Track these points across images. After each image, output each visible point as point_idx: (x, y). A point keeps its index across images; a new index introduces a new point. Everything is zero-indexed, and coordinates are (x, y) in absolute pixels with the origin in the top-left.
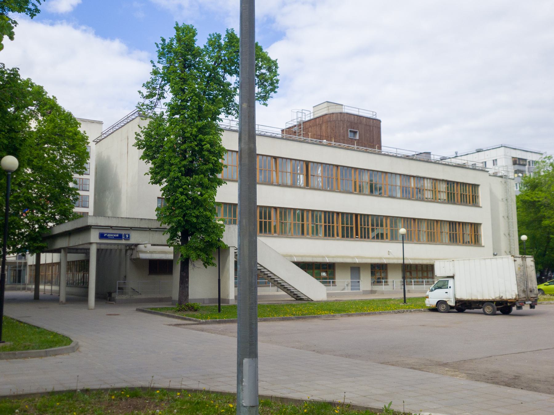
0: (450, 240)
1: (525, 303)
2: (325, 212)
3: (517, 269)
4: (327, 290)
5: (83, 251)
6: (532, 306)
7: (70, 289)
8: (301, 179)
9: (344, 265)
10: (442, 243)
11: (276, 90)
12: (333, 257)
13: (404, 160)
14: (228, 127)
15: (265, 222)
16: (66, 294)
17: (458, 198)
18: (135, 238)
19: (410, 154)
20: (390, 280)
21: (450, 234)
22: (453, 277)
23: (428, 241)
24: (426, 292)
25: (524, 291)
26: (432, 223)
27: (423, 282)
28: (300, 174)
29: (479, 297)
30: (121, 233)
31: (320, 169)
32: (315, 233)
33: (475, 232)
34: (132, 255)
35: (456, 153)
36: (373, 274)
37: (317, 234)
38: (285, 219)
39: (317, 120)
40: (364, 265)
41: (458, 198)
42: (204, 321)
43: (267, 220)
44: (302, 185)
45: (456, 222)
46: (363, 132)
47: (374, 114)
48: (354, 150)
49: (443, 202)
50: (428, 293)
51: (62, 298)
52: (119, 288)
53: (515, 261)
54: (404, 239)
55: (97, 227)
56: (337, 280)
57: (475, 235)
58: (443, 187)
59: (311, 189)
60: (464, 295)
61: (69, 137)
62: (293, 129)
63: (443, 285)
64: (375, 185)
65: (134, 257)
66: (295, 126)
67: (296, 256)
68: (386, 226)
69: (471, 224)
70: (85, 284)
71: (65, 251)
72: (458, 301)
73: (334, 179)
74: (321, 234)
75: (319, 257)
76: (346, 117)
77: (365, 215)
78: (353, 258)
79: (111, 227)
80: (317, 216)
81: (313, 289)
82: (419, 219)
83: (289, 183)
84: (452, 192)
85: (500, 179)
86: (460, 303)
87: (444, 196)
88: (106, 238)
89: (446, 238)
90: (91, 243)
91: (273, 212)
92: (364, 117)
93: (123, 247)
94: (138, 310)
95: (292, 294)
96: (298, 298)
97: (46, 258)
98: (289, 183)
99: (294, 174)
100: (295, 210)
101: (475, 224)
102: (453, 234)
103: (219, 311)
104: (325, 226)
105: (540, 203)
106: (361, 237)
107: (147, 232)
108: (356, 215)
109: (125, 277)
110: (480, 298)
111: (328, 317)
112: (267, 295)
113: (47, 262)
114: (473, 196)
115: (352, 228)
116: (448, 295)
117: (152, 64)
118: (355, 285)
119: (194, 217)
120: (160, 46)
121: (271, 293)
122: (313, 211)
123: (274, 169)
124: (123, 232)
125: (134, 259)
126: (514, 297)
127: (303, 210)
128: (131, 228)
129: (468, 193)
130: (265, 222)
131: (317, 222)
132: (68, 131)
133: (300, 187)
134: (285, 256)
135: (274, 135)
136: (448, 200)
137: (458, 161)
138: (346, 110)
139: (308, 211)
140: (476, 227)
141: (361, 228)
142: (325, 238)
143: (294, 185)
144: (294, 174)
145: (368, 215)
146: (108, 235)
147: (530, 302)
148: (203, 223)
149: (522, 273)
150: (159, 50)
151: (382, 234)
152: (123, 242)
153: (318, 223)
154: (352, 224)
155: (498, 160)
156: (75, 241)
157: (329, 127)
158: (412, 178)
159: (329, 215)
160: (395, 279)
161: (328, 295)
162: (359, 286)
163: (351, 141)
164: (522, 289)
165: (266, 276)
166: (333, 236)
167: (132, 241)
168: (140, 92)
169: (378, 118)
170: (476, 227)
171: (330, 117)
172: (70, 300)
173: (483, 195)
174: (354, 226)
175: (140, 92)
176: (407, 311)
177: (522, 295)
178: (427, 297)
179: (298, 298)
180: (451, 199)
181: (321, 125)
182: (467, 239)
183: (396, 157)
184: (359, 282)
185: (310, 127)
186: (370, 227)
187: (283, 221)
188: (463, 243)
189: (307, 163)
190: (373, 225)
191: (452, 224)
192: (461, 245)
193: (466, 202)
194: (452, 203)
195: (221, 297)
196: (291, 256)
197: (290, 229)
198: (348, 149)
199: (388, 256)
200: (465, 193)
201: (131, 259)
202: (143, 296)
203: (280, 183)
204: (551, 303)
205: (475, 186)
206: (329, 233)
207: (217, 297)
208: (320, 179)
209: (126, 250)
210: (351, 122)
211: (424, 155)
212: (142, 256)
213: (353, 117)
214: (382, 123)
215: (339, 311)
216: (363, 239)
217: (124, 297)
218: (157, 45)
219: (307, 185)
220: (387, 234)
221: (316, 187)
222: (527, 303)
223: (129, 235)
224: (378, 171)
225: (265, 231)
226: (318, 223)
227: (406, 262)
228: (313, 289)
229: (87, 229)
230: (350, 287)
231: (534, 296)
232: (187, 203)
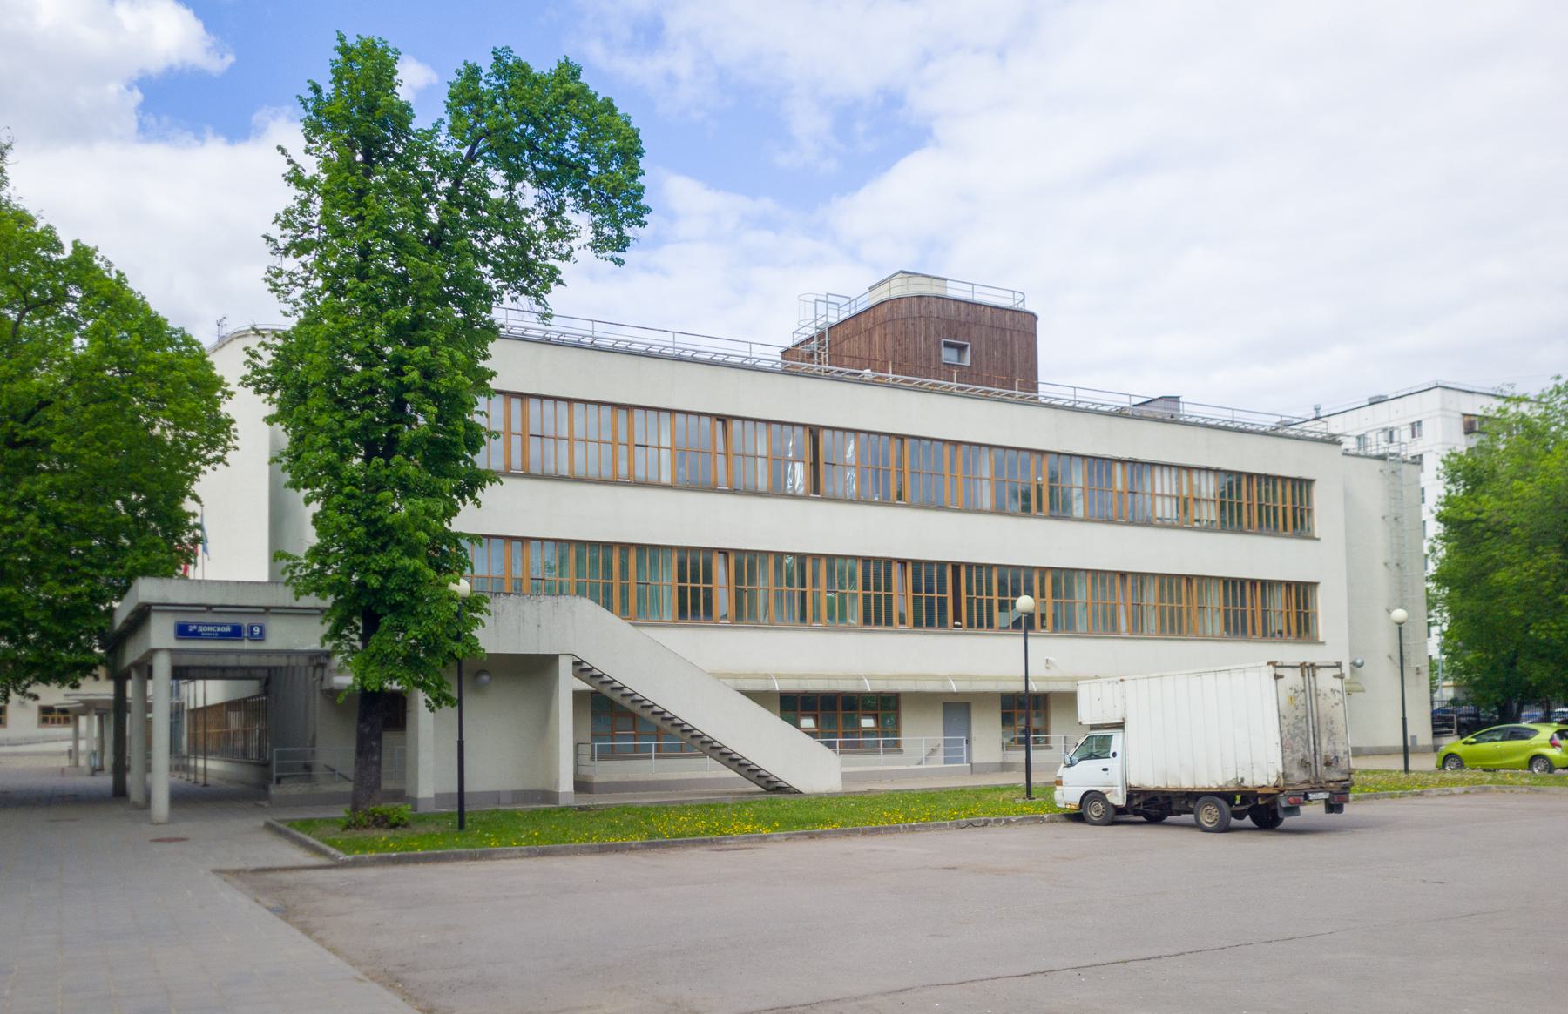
0: (1227, 628)
1: (1306, 797)
2: (866, 560)
3: (1284, 700)
4: (843, 764)
5: (238, 673)
6: (1333, 806)
8: (799, 475)
9: (924, 700)
10: (1205, 638)
11: (645, 218)
12: (888, 678)
14: (588, 341)
15: (695, 591)
17: (1250, 514)
19: (1124, 402)
21: (1226, 612)
22: (1120, 726)
23: (1163, 630)
24: (1056, 768)
25: (1304, 764)
26: (1172, 583)
28: (793, 461)
29: (1184, 781)
31: (852, 447)
32: (837, 616)
33: (1298, 606)
35: (1317, 409)
36: (1007, 719)
37: (843, 618)
38: (752, 580)
39: (863, 318)
40: (983, 697)
41: (1250, 514)
42: (350, 857)
43: (701, 585)
44: (801, 491)
45: (1243, 581)
46: (988, 346)
48: (951, 394)
49: (1209, 528)
50: (1062, 772)
53: (1277, 677)
54: (1026, 624)
55: (168, 608)
56: (905, 738)
57: (1298, 615)
59: (824, 499)
60: (1150, 779)
61: (146, 377)
62: (805, 349)
63: (1097, 746)
64: (1037, 487)
65: (326, 686)
66: (812, 338)
67: (779, 677)
69: (1288, 584)
72: (1132, 794)
73: (893, 474)
74: (855, 617)
75: (847, 677)
76: (933, 307)
77: (980, 566)
78: (944, 679)
79: (210, 607)
80: (842, 572)
81: (807, 762)
82: (1264, 583)
83: (762, 484)
84: (1235, 500)
85: (1379, 464)
86: (1142, 799)
87: (1210, 513)
88: (196, 635)
89: (1215, 623)
91: (896, 568)
94: (269, 827)
95: (754, 776)
96: (771, 786)
98: (762, 484)
99: (778, 463)
100: (780, 555)
102: (1235, 612)
103: (461, 825)
104: (866, 598)
105: (1482, 525)
106: (970, 625)
108: (956, 567)
110: (1187, 784)
112: (698, 780)
113: (210, 702)
114: (1294, 510)
115: (942, 602)
116: (1110, 778)
117: (285, 159)
119: (375, 572)
120: (310, 105)
121: (708, 775)
122: (831, 558)
123: (720, 448)
124: (245, 622)
126: (1273, 780)
127: (801, 558)
128: (267, 610)
129: (1280, 504)
130: (695, 591)
131: (842, 586)
132: (147, 363)
133: (794, 496)
134: (718, 676)
135: (719, 358)
136: (1223, 522)
137: (1319, 427)
138: (955, 291)
139: (817, 557)
140: (1302, 593)
141: (970, 602)
142: (867, 628)
143: (777, 491)
144: (778, 463)
145: (990, 567)
146: (201, 629)
147: (1326, 796)
148: (401, 589)
149: (1301, 713)
150: (309, 118)
153: (847, 590)
154: (942, 589)
155: (1424, 424)
157: (889, 337)
158: (1118, 466)
159: (877, 569)
161: (846, 777)
163: (946, 371)
164: (1299, 756)
168: (268, 238)
169: (1029, 307)
170: (1302, 593)
171: (891, 310)
173: (1325, 508)
174: (949, 595)
175: (268, 238)
176: (998, 821)
177: (1299, 775)
178: (1059, 783)
179: (773, 787)
181: (870, 332)
182: (1278, 623)
183: (1073, 409)
185: (847, 338)
186: (996, 598)
187: (745, 586)
188: (1265, 635)
189: (814, 431)
190: (1003, 592)
191: (1234, 586)
192: (1255, 641)
193: (1276, 526)
194: (1233, 531)
195: (467, 789)
196: (735, 677)
197: (767, 607)
198: (931, 392)
199: (1047, 674)
200: (1271, 503)
204: (1452, 794)
205: (1302, 485)
206: (877, 616)
207: (456, 790)
208: (851, 474)
210: (950, 322)
211: (1161, 403)
213: (953, 307)
214: (1039, 323)
218: (304, 103)
219: (815, 488)
221: (840, 493)
222: (1312, 796)
224: (932, 440)
225: (695, 614)
226: (847, 590)
227: (1034, 687)
230: (940, 755)
231: (1337, 777)
232: (352, 535)
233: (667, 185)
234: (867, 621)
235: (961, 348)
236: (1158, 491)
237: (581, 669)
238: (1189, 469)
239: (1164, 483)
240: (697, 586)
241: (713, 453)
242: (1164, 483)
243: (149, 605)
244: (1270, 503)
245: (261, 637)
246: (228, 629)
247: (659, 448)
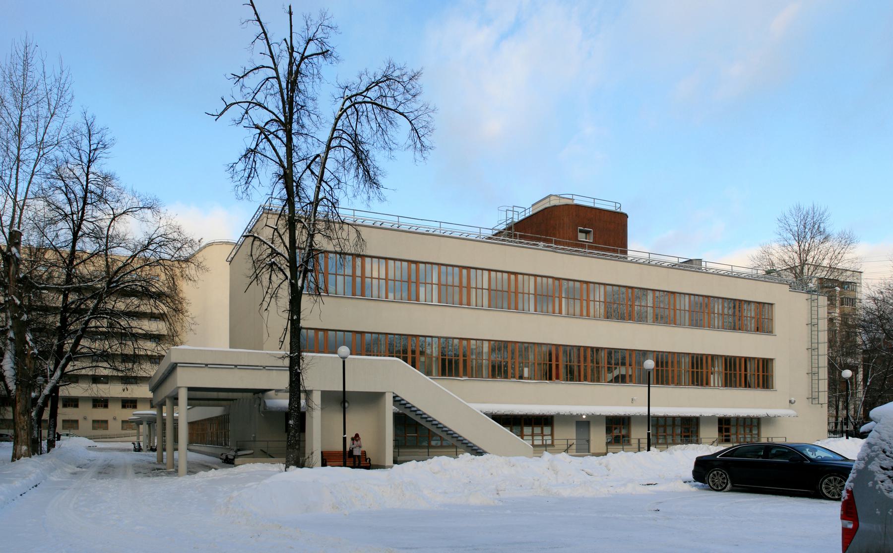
13: (224, 245)
36: (609, 430)
46: (604, 230)
47: (618, 205)
64: (624, 304)
95: (598, 436)
140: (765, 365)
163: (582, 245)
169: (623, 210)
170: (765, 365)
183: (649, 264)
203: (672, 296)
220: (672, 362)
233: (406, 63)
235: (587, 233)
237: (397, 400)
240: (452, 362)
241: (553, 297)
243: (176, 364)
244: (751, 316)
247: (432, 284)
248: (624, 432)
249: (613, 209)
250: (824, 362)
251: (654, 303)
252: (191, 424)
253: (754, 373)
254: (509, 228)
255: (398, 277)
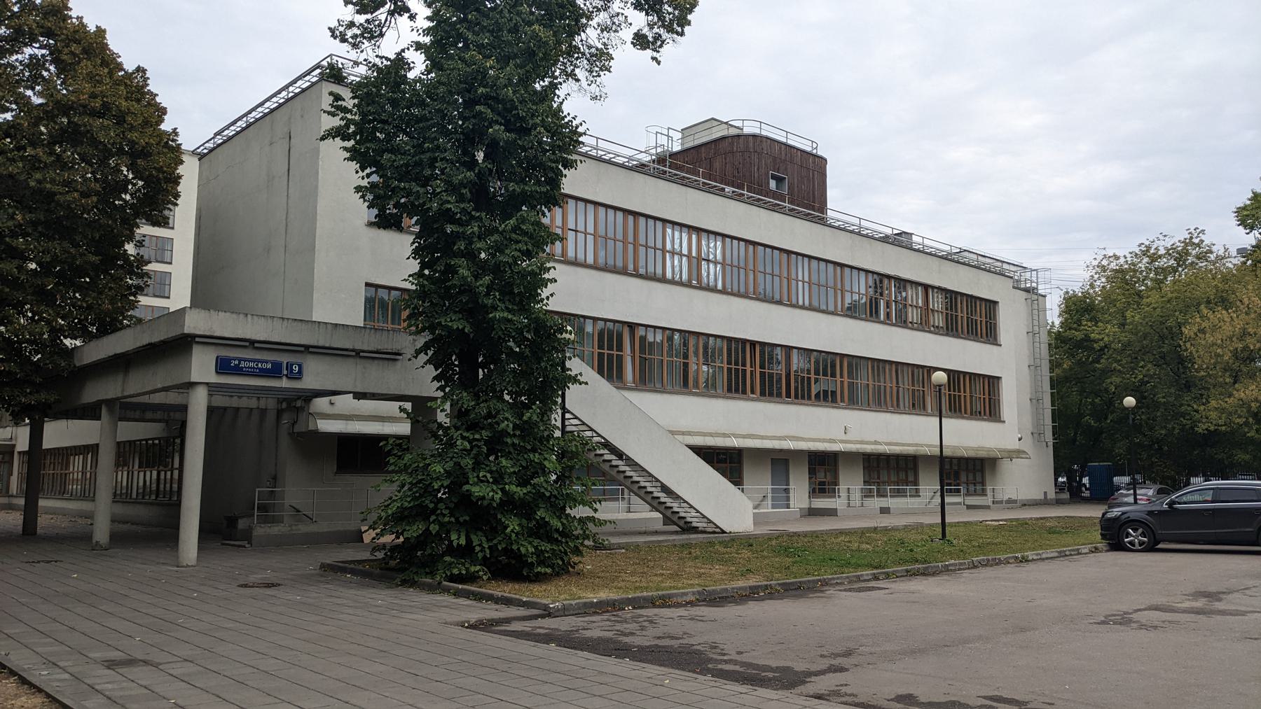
2: (729, 339)
7: (120, 509)
9: (760, 454)
16: (113, 521)
18: (315, 374)
20: (842, 487)
23: (729, 390)
27: (904, 491)
30: (281, 358)
34: (295, 422)
36: (812, 472)
46: (789, 177)
51: (101, 533)
52: (263, 508)
58: (937, 302)
65: (297, 429)
68: (842, 376)
70: (171, 504)
71: (111, 411)
81: (731, 508)
85: (1024, 294)
87: (939, 320)
88: (238, 371)
90: (192, 385)
92: (798, 149)
93: (271, 404)
97: (57, 434)
101: (989, 377)
107: (351, 360)
109: (275, 478)
111: (856, 585)
118: (782, 497)
124: (284, 359)
125: (300, 434)
128: (307, 349)
140: (992, 382)
151: (834, 393)
152: (284, 383)
156: (138, 384)
160: (851, 483)
161: (757, 520)
162: (788, 499)
165: (622, 476)
166: (744, 392)
167: (310, 381)
172: (123, 538)
180: (951, 329)
183: (859, 234)
184: (787, 491)
199: (844, 438)
201: (292, 434)
202: (323, 527)
209: (279, 413)
210: (775, 159)
212: (326, 426)
215: (914, 574)
216: (800, 401)
217: (275, 530)
223: (300, 366)
228: (731, 508)
229: (181, 345)
234: (729, 390)
236: (669, 247)
238: (698, 230)
239: (802, 271)
242: (678, 240)
244: (971, 317)
245: (299, 376)
246: (269, 366)
248: (829, 478)
249: (809, 149)
250: (690, 674)
251: (64, 454)
252: (211, 410)
253: (973, 395)
254: (661, 160)
255: (581, 236)
